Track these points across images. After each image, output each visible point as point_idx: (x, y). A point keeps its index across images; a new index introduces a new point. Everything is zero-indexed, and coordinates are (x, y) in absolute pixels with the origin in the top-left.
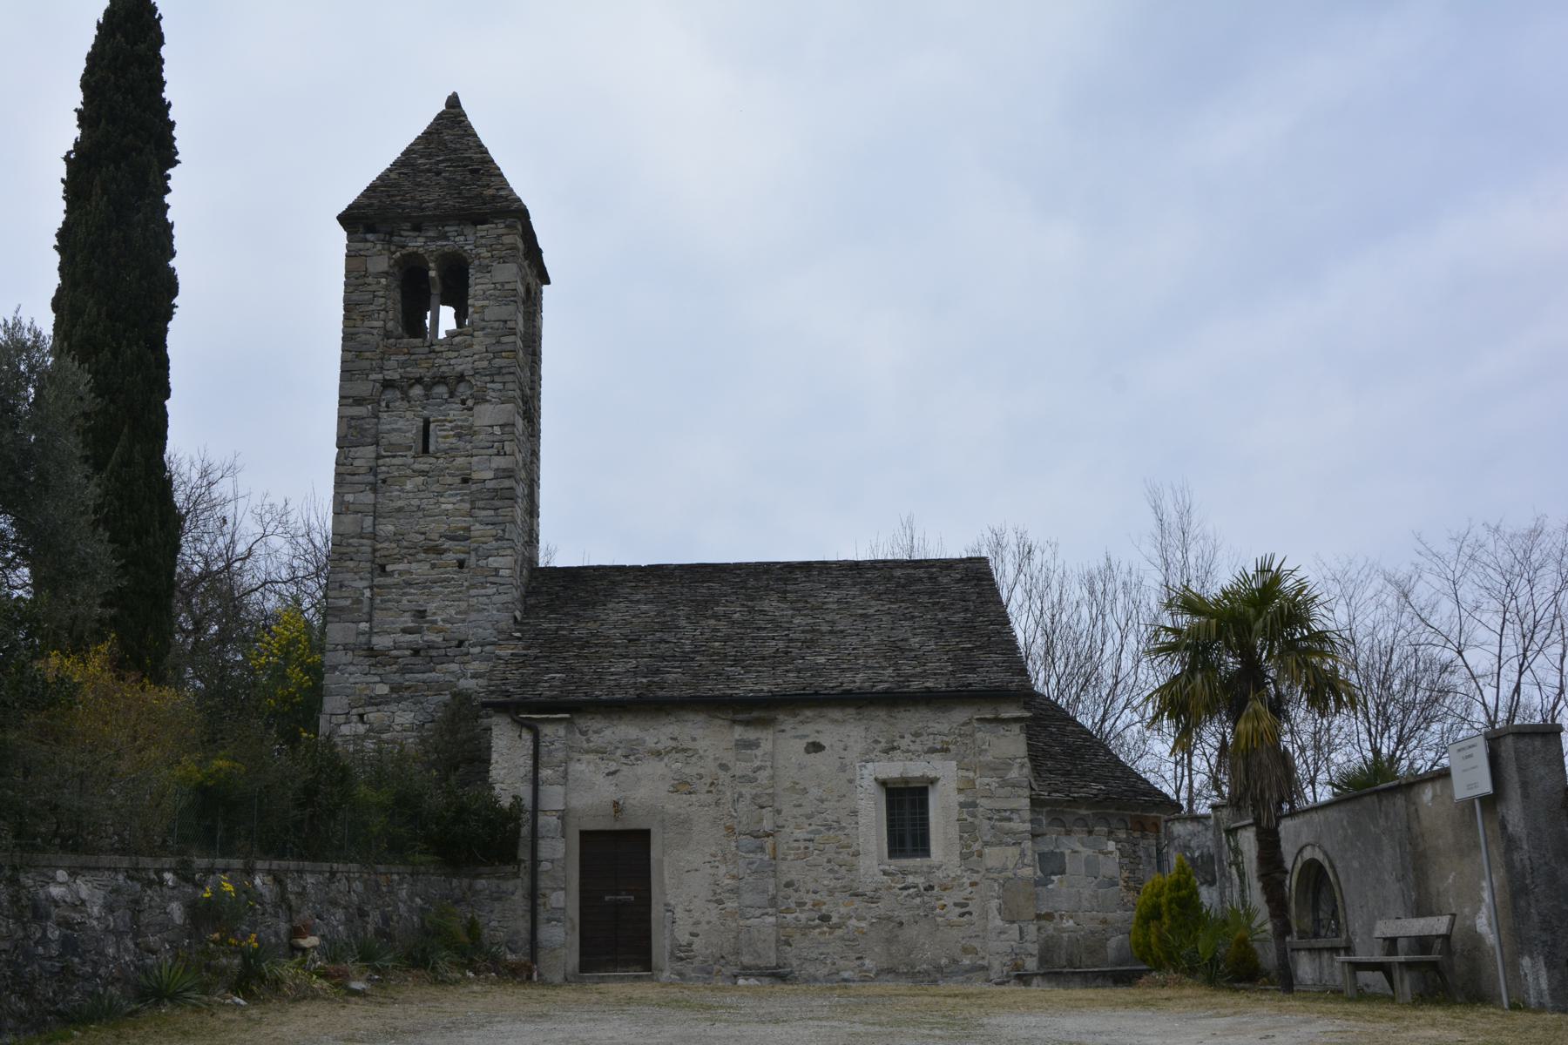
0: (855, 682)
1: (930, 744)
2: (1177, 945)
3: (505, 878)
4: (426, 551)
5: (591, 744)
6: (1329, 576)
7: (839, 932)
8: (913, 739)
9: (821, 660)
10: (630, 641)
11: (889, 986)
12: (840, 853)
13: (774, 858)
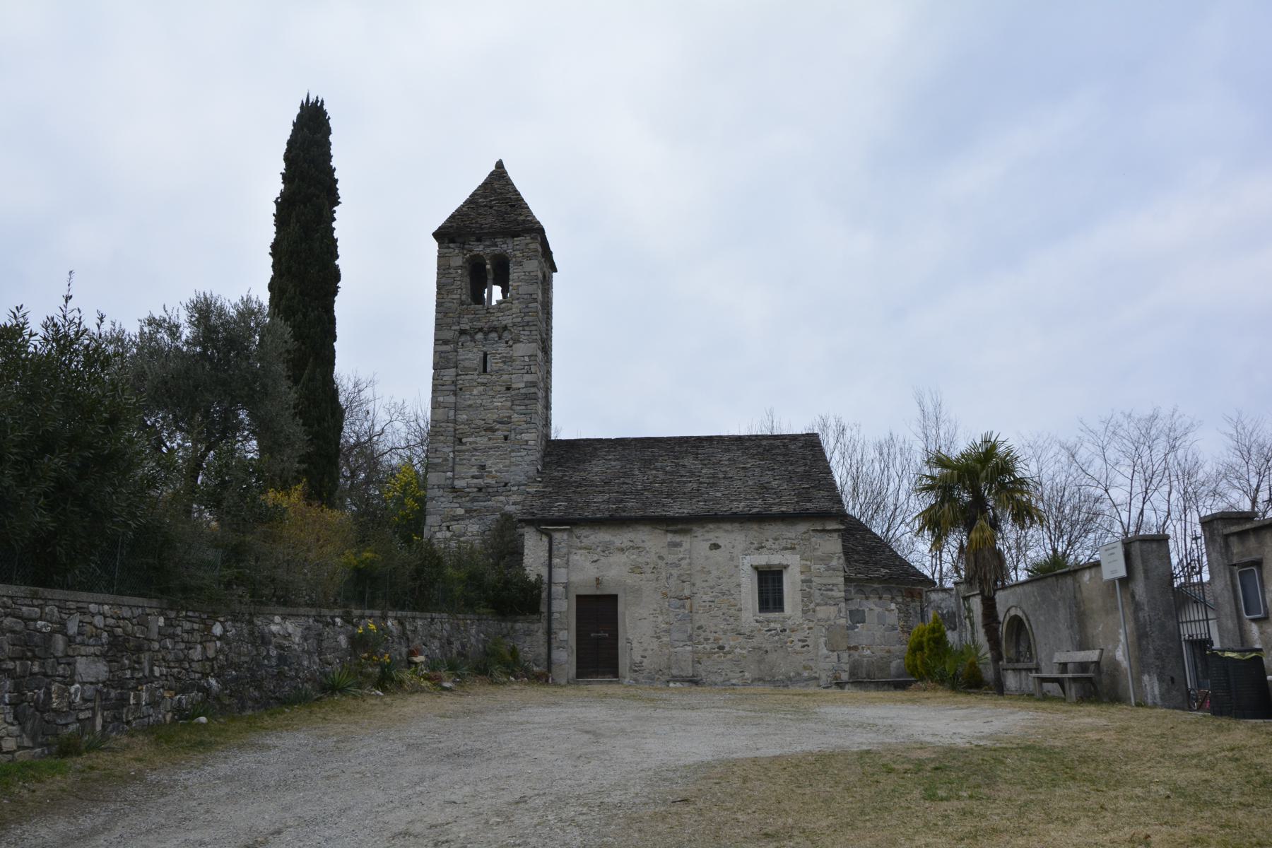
3: (532, 623)
4: (486, 430)
6: (1026, 444)
7: (729, 656)
9: (719, 494)
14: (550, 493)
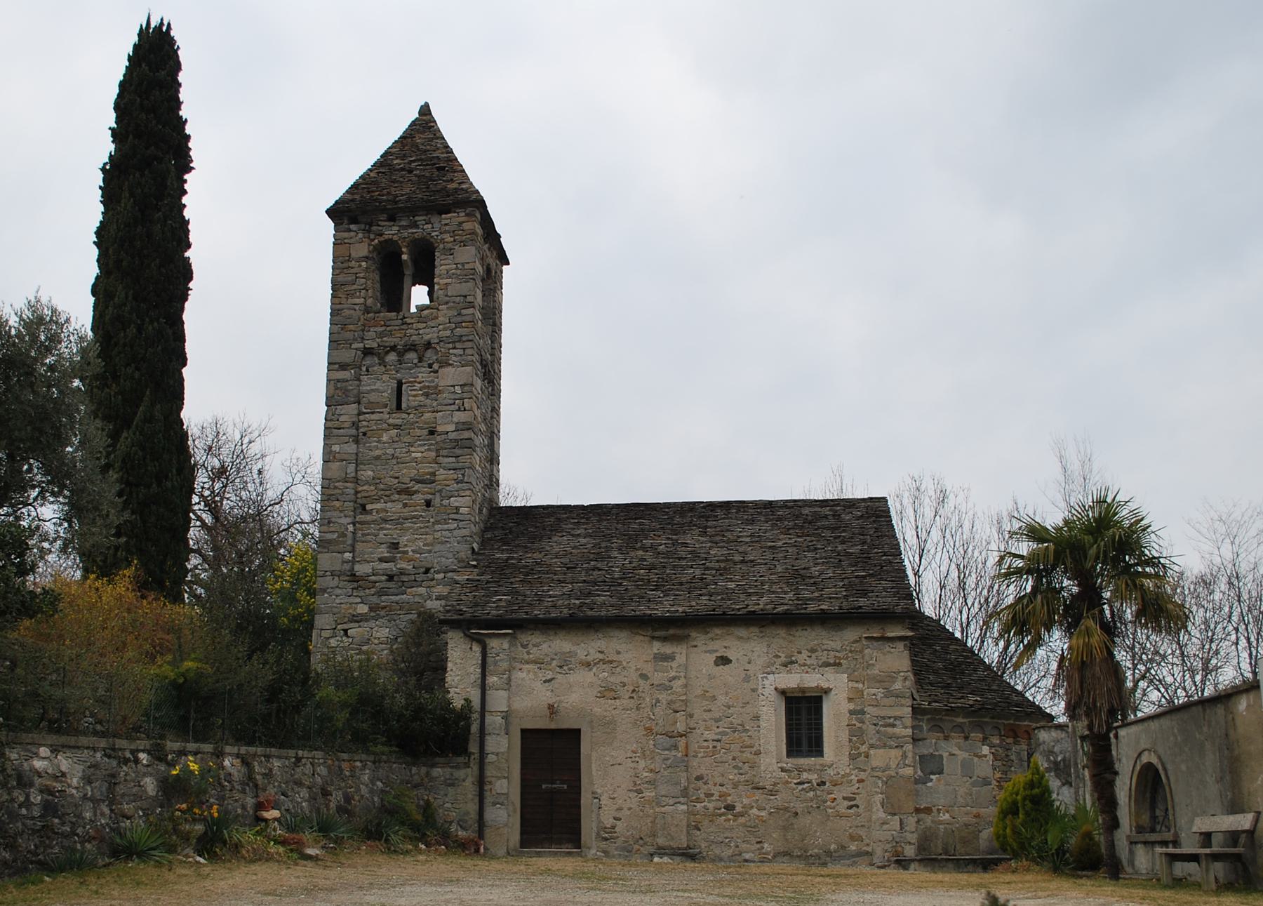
0: (759, 604)
1: (824, 659)
2: (1029, 836)
3: (457, 767)
4: (399, 493)
5: (531, 656)
6: (1216, 517)
7: (742, 820)
8: (809, 654)
9: (732, 585)
10: (568, 568)
11: (777, 867)
12: (743, 752)
13: (687, 756)
14: (488, 582)
